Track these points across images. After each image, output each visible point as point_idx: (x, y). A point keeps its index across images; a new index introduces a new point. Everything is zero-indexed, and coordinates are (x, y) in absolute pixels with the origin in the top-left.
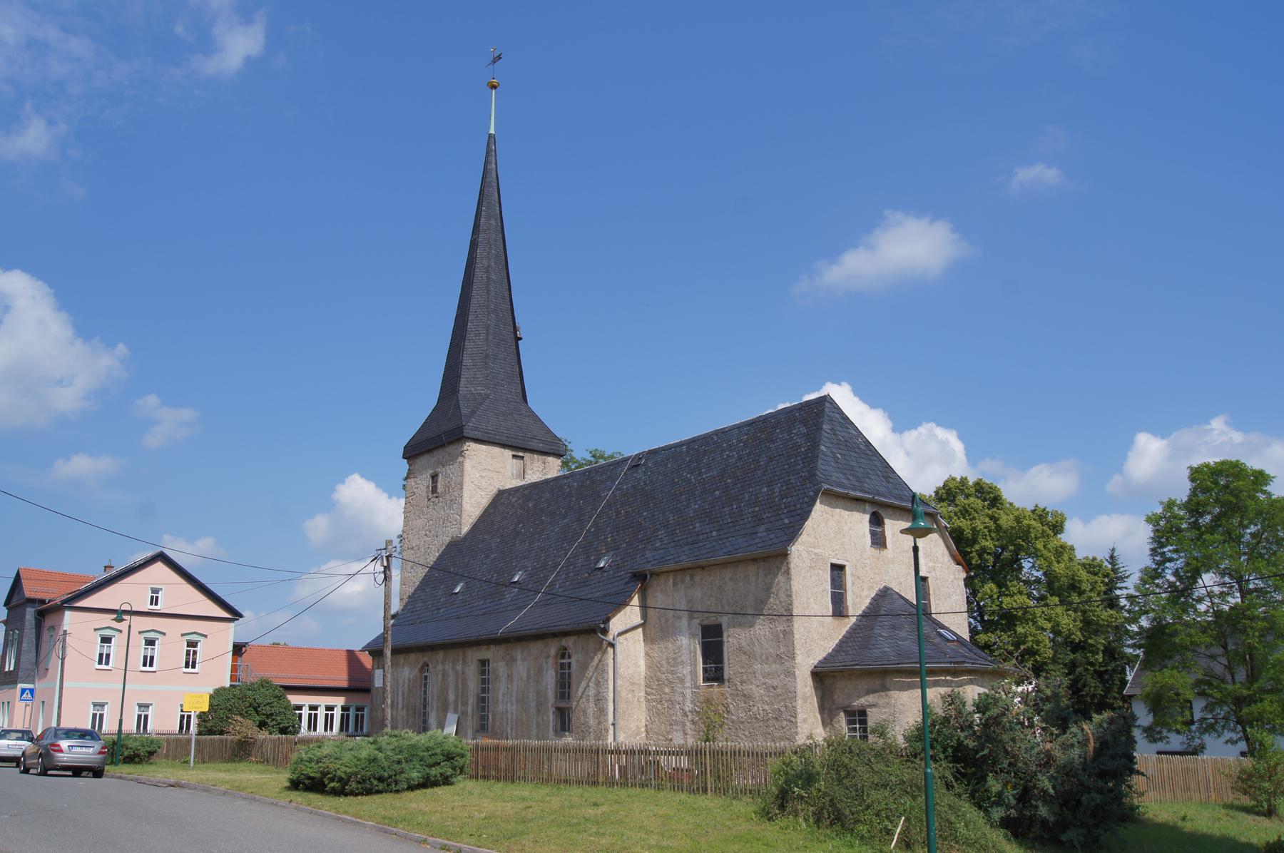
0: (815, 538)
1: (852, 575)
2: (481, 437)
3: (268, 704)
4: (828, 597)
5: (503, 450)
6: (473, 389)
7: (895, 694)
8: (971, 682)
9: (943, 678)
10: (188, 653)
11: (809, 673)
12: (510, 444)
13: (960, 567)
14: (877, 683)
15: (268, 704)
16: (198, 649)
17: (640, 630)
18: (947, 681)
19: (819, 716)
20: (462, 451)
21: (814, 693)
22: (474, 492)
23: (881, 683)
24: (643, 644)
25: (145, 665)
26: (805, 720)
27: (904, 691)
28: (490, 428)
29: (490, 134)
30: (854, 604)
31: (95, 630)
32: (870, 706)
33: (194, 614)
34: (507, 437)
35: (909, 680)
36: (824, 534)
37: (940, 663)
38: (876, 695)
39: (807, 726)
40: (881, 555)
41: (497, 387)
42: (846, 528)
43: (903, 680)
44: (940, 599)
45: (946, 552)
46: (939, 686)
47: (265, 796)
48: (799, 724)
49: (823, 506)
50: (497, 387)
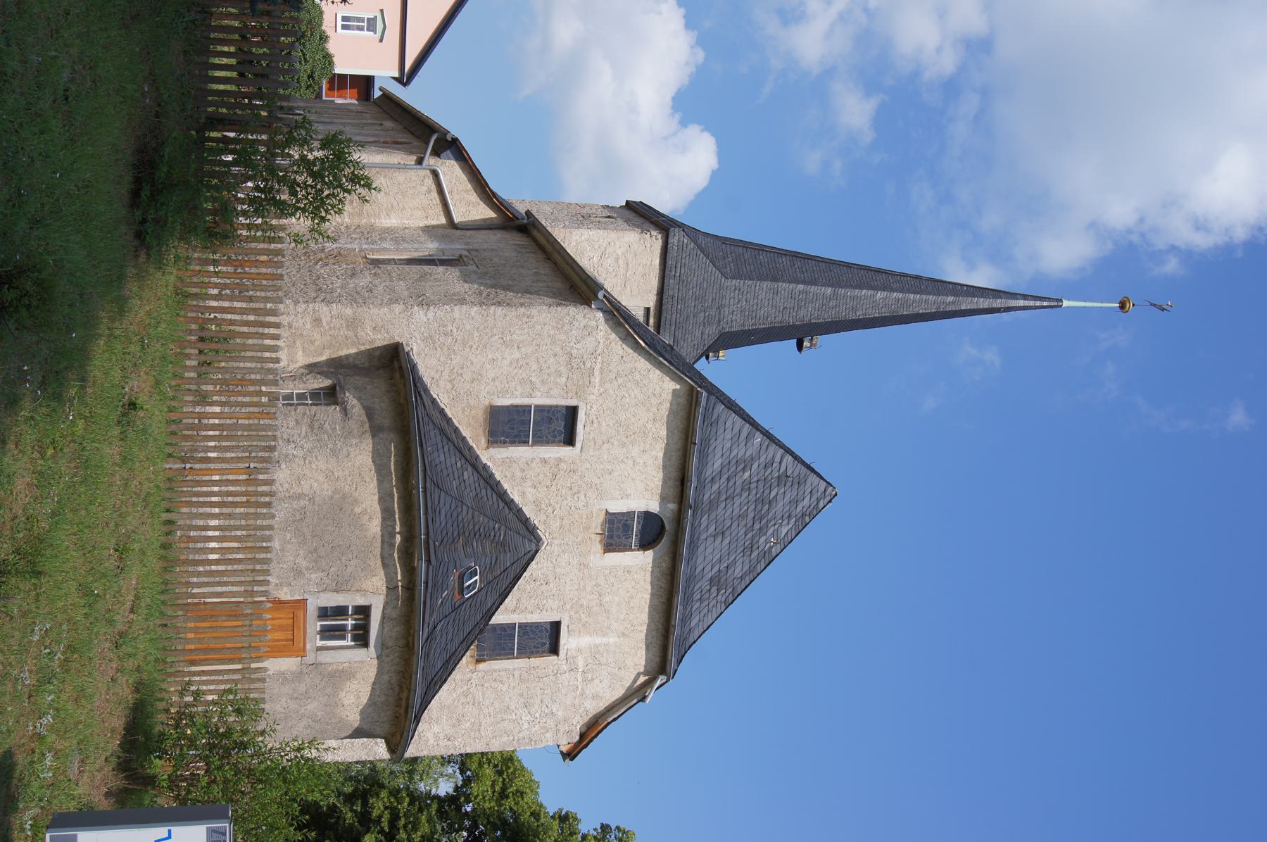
0: (618, 374)
1: (560, 460)
2: (669, 255)
3: (304, 55)
4: (522, 395)
5: (655, 292)
6: (730, 259)
7: (367, 444)
8: (391, 589)
9: (398, 529)
10: (360, 20)
11: (397, 339)
12: (664, 301)
13: (577, 738)
14: (385, 419)
15: (304, 55)
16: (366, 33)
17: (443, 221)
18: (392, 535)
19: (324, 358)
20: (649, 231)
21: (363, 348)
22: (596, 247)
23: (386, 426)
24: (422, 224)
25: (344, 19)
26: (317, 321)
27: (373, 457)
28: (683, 271)
29: (1061, 301)
30: (511, 461)
31: (382, 11)
32: (345, 412)
33: (407, 28)
34: (673, 296)
35: (393, 467)
36: (623, 396)
37: (426, 513)
38: (364, 418)
39: (308, 326)
40: (593, 536)
41: (737, 291)
42: (635, 451)
43: (392, 458)
44: (522, 680)
45: (602, 705)
46: (384, 519)
47: (171, 444)
48: (311, 305)
49: (670, 397)
50: (737, 291)
